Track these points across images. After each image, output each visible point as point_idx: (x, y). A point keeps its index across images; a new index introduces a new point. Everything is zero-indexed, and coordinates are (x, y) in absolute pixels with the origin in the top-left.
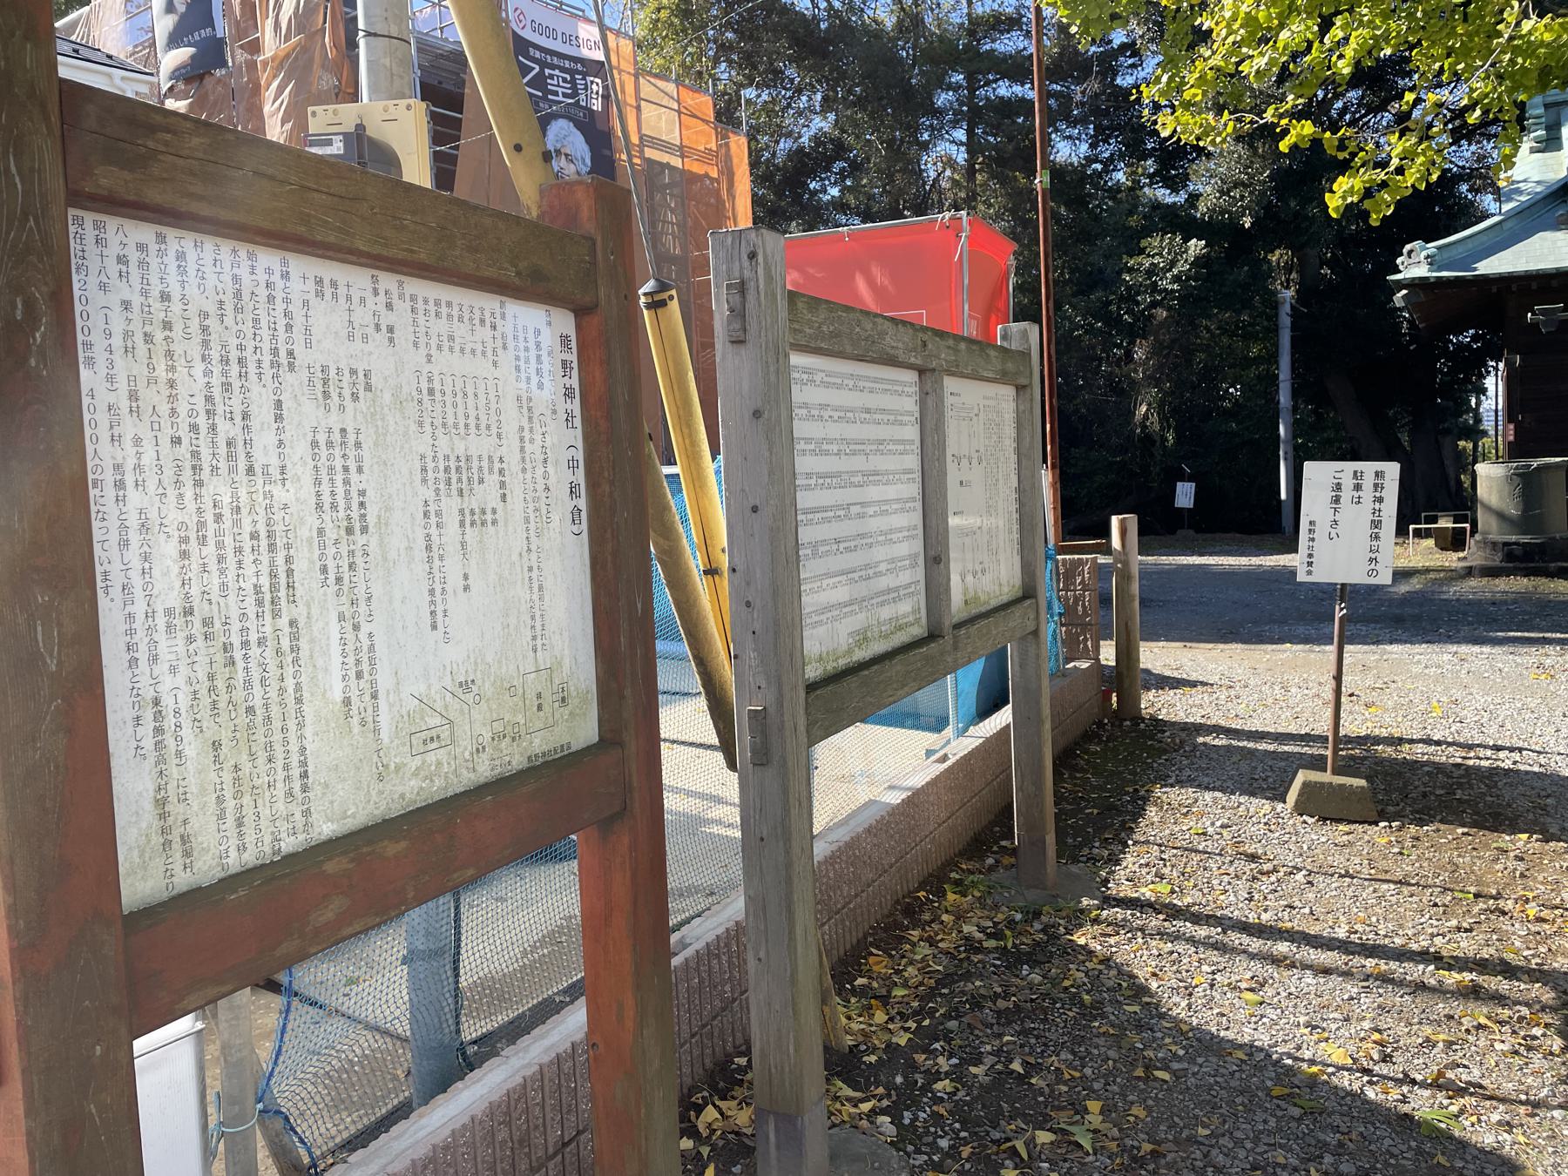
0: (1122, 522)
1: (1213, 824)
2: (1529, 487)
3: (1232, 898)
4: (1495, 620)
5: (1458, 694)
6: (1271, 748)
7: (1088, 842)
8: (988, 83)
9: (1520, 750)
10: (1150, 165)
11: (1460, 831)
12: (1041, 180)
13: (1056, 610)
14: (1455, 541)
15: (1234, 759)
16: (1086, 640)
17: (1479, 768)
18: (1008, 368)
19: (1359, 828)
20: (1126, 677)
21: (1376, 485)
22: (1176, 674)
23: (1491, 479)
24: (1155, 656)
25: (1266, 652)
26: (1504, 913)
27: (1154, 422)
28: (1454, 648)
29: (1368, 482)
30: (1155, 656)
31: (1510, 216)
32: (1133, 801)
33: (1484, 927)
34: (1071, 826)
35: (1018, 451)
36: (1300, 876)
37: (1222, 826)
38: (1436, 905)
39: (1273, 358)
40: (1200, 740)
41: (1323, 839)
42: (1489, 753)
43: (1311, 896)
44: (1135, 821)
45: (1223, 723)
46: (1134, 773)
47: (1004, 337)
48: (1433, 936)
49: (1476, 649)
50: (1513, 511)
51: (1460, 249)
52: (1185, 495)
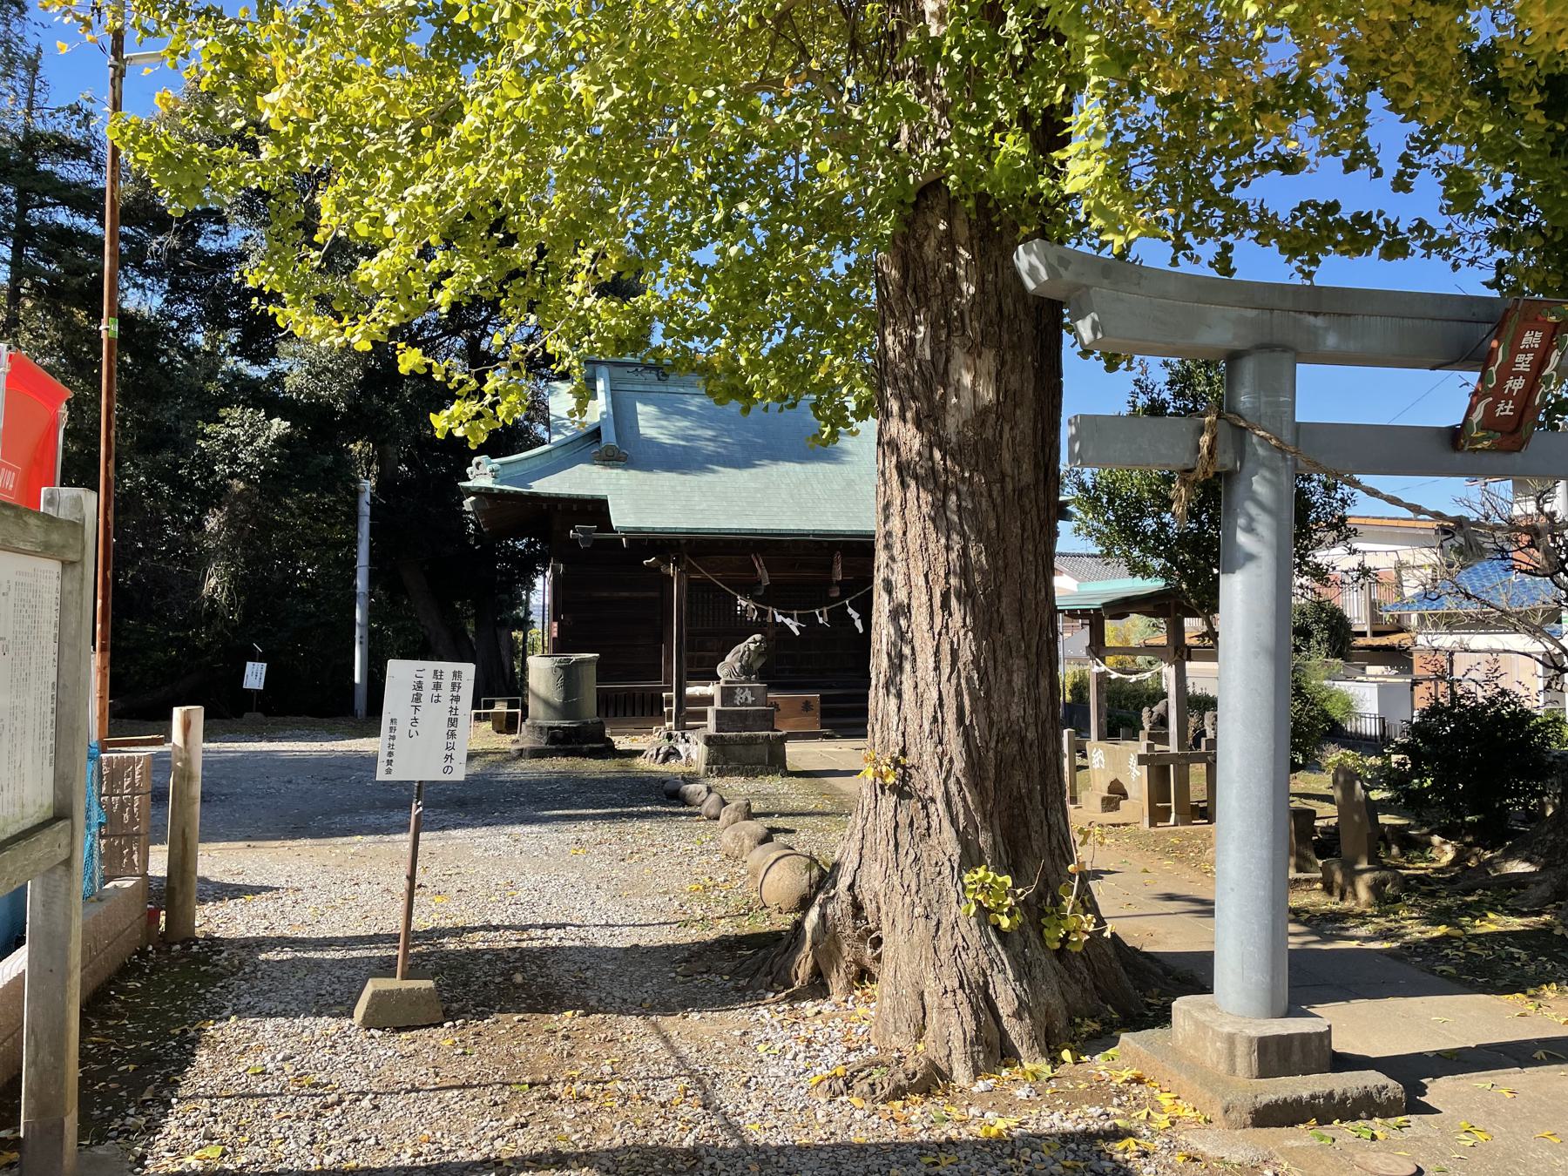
0: (186, 714)
1: (273, 1058)
2: (569, 677)
3: (293, 1145)
4: (542, 800)
5: (512, 875)
6: (338, 955)
7: (120, 1111)
8: (42, 205)
9: (564, 926)
10: (234, 336)
11: (516, 1018)
12: (108, 328)
13: (95, 820)
14: (508, 725)
15: (300, 975)
16: (131, 853)
17: (531, 950)
18: (56, 540)
19: (425, 1032)
20: (178, 891)
21: (453, 685)
22: (238, 881)
23: (541, 672)
24: (216, 861)
25: (335, 846)
26: (554, 1098)
27: (222, 597)
28: (508, 829)
29: (447, 681)
30: (216, 861)
31: (563, 445)
32: (181, 1045)
33: (538, 1118)
34: (99, 1093)
35: (60, 641)
36: (366, 1103)
37: (284, 1060)
38: (496, 1104)
39: (353, 543)
40: (263, 956)
41: (390, 1053)
42: (539, 932)
43: (377, 1122)
44: (181, 1071)
45: (288, 933)
46: (182, 1010)
47: (50, 502)
48: (493, 1139)
49: (527, 829)
50: (557, 699)
51: (518, 468)
52: (255, 676)
